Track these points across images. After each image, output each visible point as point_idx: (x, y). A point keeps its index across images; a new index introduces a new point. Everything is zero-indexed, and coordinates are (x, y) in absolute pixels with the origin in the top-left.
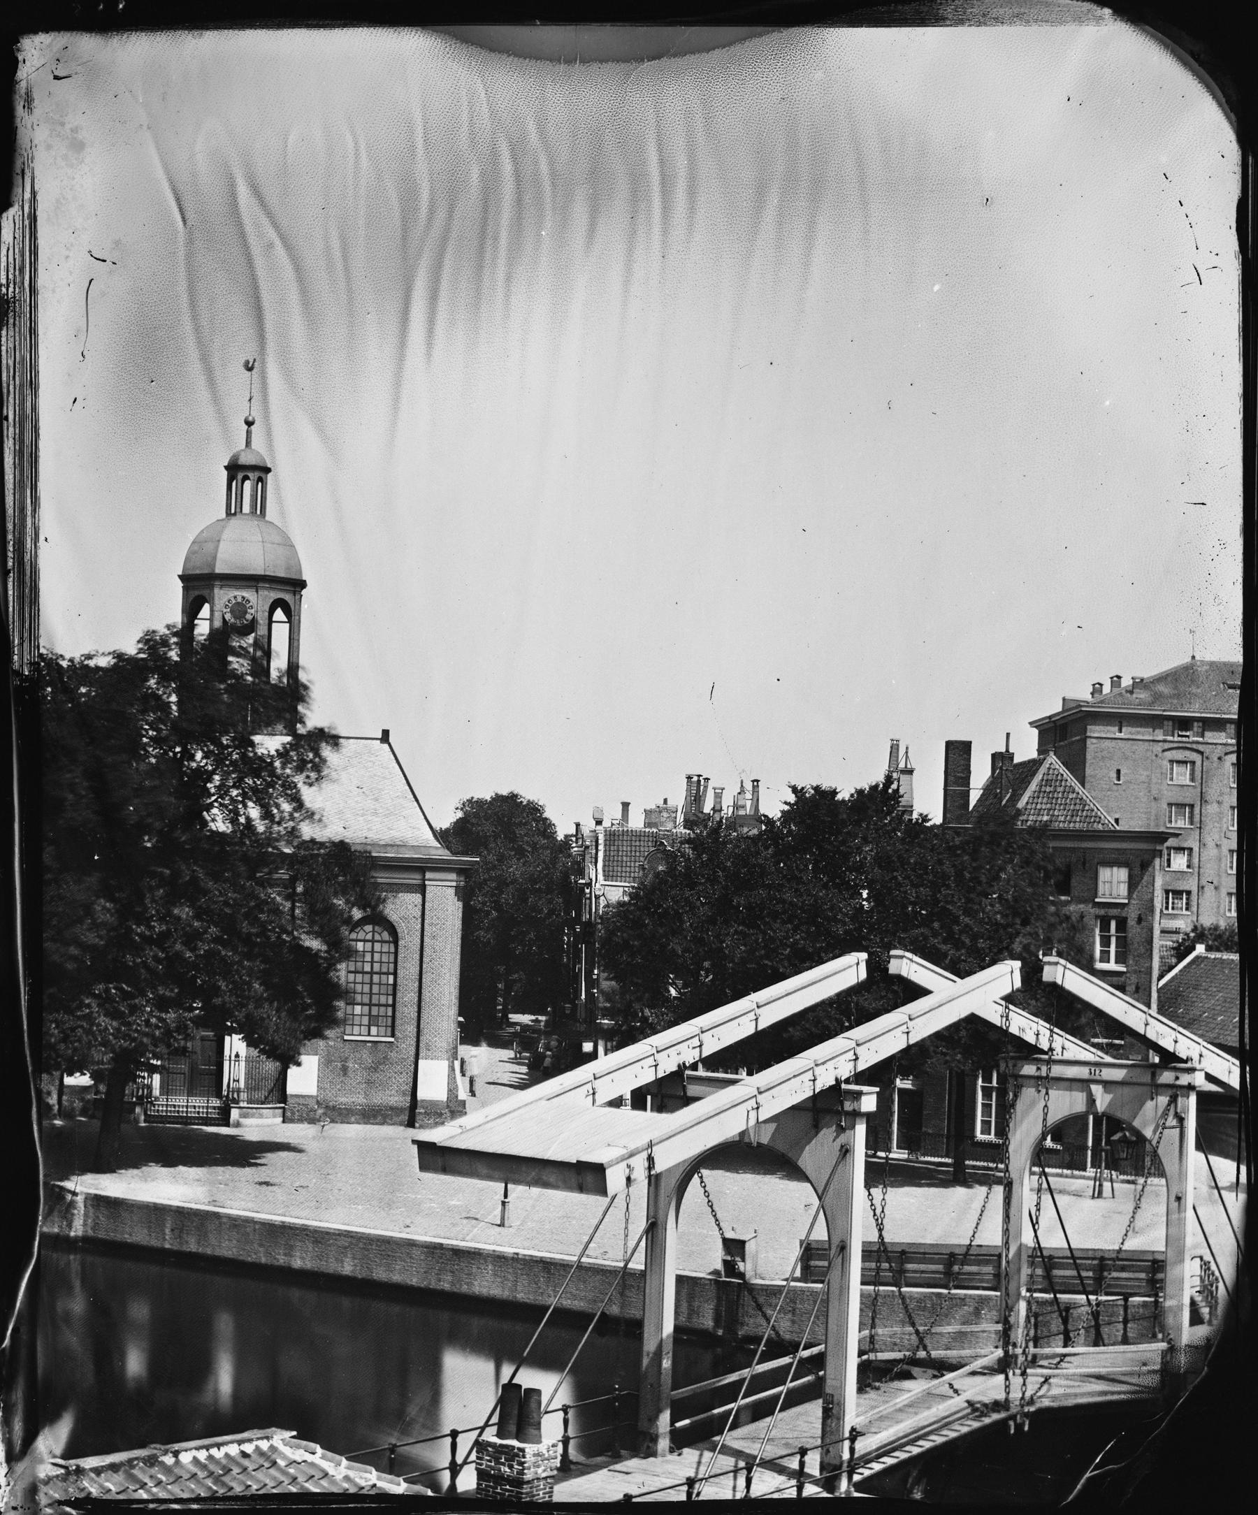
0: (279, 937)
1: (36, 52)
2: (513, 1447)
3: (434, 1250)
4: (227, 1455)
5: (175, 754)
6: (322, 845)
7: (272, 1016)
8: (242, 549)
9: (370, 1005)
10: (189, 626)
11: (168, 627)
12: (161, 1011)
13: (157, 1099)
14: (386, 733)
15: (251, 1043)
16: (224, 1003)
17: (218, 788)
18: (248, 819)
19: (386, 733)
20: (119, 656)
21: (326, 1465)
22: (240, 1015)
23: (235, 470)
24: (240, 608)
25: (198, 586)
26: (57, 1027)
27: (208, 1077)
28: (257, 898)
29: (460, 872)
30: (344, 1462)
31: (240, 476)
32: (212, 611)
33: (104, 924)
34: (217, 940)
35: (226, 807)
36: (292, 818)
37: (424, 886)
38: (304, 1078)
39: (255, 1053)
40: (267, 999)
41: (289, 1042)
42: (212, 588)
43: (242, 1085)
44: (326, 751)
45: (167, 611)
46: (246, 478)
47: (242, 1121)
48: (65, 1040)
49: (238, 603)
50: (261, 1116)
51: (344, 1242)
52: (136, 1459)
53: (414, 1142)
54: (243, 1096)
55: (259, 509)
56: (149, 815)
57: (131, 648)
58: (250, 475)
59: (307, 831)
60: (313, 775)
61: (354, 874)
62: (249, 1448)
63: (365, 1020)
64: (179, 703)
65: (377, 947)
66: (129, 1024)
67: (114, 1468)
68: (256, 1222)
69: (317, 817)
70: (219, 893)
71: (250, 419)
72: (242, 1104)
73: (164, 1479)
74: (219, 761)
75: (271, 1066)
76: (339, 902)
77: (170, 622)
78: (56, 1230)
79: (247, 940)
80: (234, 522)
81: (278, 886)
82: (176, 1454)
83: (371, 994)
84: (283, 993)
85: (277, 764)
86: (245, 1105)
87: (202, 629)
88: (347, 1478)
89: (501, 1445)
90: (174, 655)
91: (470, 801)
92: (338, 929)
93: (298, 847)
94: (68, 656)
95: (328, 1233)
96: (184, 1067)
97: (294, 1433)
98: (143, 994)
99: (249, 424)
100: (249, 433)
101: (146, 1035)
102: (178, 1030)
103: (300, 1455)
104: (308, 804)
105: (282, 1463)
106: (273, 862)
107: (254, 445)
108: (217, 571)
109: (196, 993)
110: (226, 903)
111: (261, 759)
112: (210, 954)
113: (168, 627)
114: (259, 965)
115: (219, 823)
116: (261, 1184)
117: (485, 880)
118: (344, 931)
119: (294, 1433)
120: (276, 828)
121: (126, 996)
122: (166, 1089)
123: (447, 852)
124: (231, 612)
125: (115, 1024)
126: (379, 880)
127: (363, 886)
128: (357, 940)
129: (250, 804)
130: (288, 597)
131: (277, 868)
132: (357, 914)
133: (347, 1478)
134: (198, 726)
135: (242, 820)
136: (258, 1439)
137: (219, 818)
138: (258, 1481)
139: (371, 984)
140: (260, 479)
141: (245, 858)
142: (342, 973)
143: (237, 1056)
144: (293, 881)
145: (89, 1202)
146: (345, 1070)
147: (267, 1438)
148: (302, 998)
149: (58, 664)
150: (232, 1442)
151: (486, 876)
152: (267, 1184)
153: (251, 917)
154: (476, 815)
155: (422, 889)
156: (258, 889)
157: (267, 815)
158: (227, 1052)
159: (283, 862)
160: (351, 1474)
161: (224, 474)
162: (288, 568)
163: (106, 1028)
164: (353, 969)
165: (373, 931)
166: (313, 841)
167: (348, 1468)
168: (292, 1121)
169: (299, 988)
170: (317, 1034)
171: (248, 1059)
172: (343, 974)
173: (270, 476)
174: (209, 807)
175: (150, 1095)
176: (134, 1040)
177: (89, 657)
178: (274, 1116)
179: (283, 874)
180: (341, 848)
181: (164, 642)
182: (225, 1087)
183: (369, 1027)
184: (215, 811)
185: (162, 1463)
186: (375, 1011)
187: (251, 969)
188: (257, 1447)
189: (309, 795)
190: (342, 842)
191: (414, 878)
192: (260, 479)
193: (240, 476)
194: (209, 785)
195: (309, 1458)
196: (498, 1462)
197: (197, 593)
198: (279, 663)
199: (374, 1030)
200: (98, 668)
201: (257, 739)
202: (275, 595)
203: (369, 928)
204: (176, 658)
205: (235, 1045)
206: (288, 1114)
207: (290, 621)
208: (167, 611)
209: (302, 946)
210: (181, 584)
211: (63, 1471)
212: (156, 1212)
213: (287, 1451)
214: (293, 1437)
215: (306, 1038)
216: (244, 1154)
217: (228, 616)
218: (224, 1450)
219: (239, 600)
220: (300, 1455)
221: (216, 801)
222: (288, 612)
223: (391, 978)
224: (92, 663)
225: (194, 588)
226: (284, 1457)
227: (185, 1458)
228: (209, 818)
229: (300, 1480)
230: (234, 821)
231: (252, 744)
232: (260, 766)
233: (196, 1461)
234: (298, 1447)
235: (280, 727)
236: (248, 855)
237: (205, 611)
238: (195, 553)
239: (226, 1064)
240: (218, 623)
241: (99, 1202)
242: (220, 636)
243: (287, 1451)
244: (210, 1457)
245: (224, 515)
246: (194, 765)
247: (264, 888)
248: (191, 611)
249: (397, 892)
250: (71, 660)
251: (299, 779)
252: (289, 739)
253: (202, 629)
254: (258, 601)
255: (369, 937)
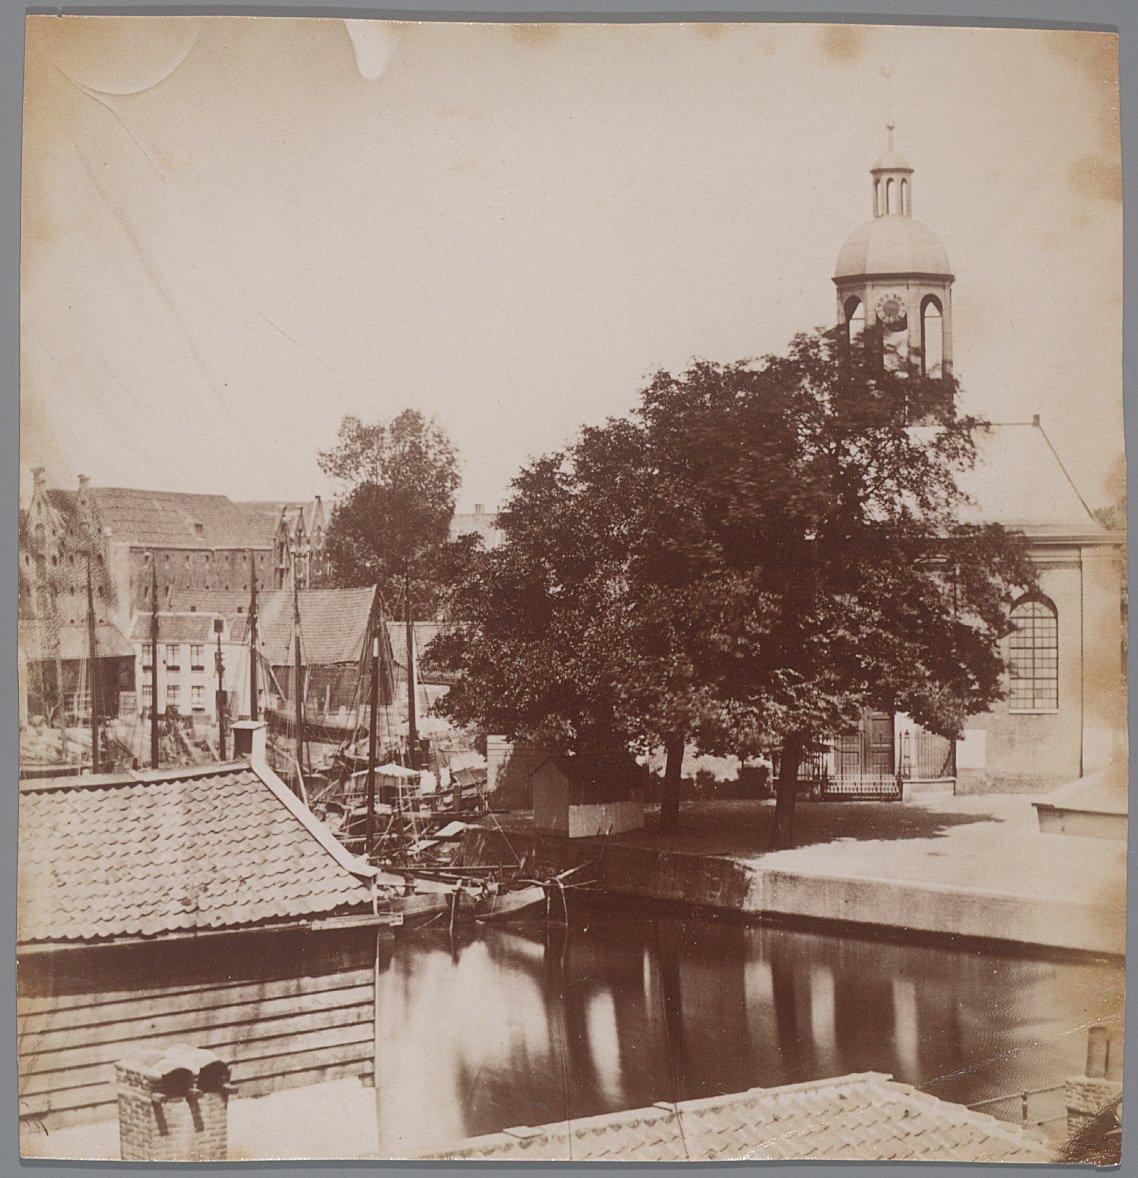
1: (43, 39)
5: (830, 450)
8: (890, 249)
10: (845, 327)
12: (827, 693)
13: (832, 777)
14: (1037, 417)
16: (887, 683)
19: (1037, 417)
24: (891, 307)
25: (850, 287)
28: (915, 580)
34: (880, 624)
35: (882, 497)
36: (948, 503)
37: (1081, 562)
41: (952, 719)
48: (736, 724)
49: (890, 302)
52: (737, 1101)
53: (1033, 805)
55: (905, 208)
57: (784, 352)
59: (964, 515)
62: (845, 1091)
71: (891, 125)
72: (912, 780)
74: (875, 455)
75: (940, 743)
76: (996, 580)
77: (818, 325)
79: (910, 621)
81: (937, 569)
84: (945, 671)
90: (825, 355)
92: (995, 607)
94: (723, 363)
96: (858, 746)
97: (891, 1076)
98: (809, 678)
102: (845, 711)
105: (876, 1104)
110: (886, 589)
118: (1005, 608)
121: (793, 680)
122: (841, 769)
125: (784, 708)
127: (1018, 566)
134: (854, 420)
135: (898, 509)
141: (903, 545)
142: (1004, 648)
143: (907, 733)
144: (951, 562)
145: (767, 879)
146: (1011, 741)
152: (937, 854)
153: (912, 600)
156: (918, 575)
165: (1034, 609)
173: (913, 175)
176: (803, 722)
177: (743, 363)
178: (947, 789)
182: (897, 765)
184: (871, 501)
189: (961, 480)
192: (904, 180)
194: (865, 477)
197: (850, 294)
198: (933, 358)
200: (753, 373)
203: (1029, 605)
206: (958, 787)
207: (942, 315)
216: (925, 825)
217: (881, 314)
219: (891, 298)
221: (872, 492)
222: (939, 306)
224: (747, 369)
225: (849, 289)
228: (865, 508)
230: (891, 511)
232: (915, 457)
233: (794, 1104)
235: (931, 418)
236: (905, 542)
237: (859, 312)
240: (872, 322)
244: (809, 1099)
245: (870, 215)
246: (849, 459)
247: (923, 572)
251: (952, 466)
253: (856, 327)
254: (909, 297)
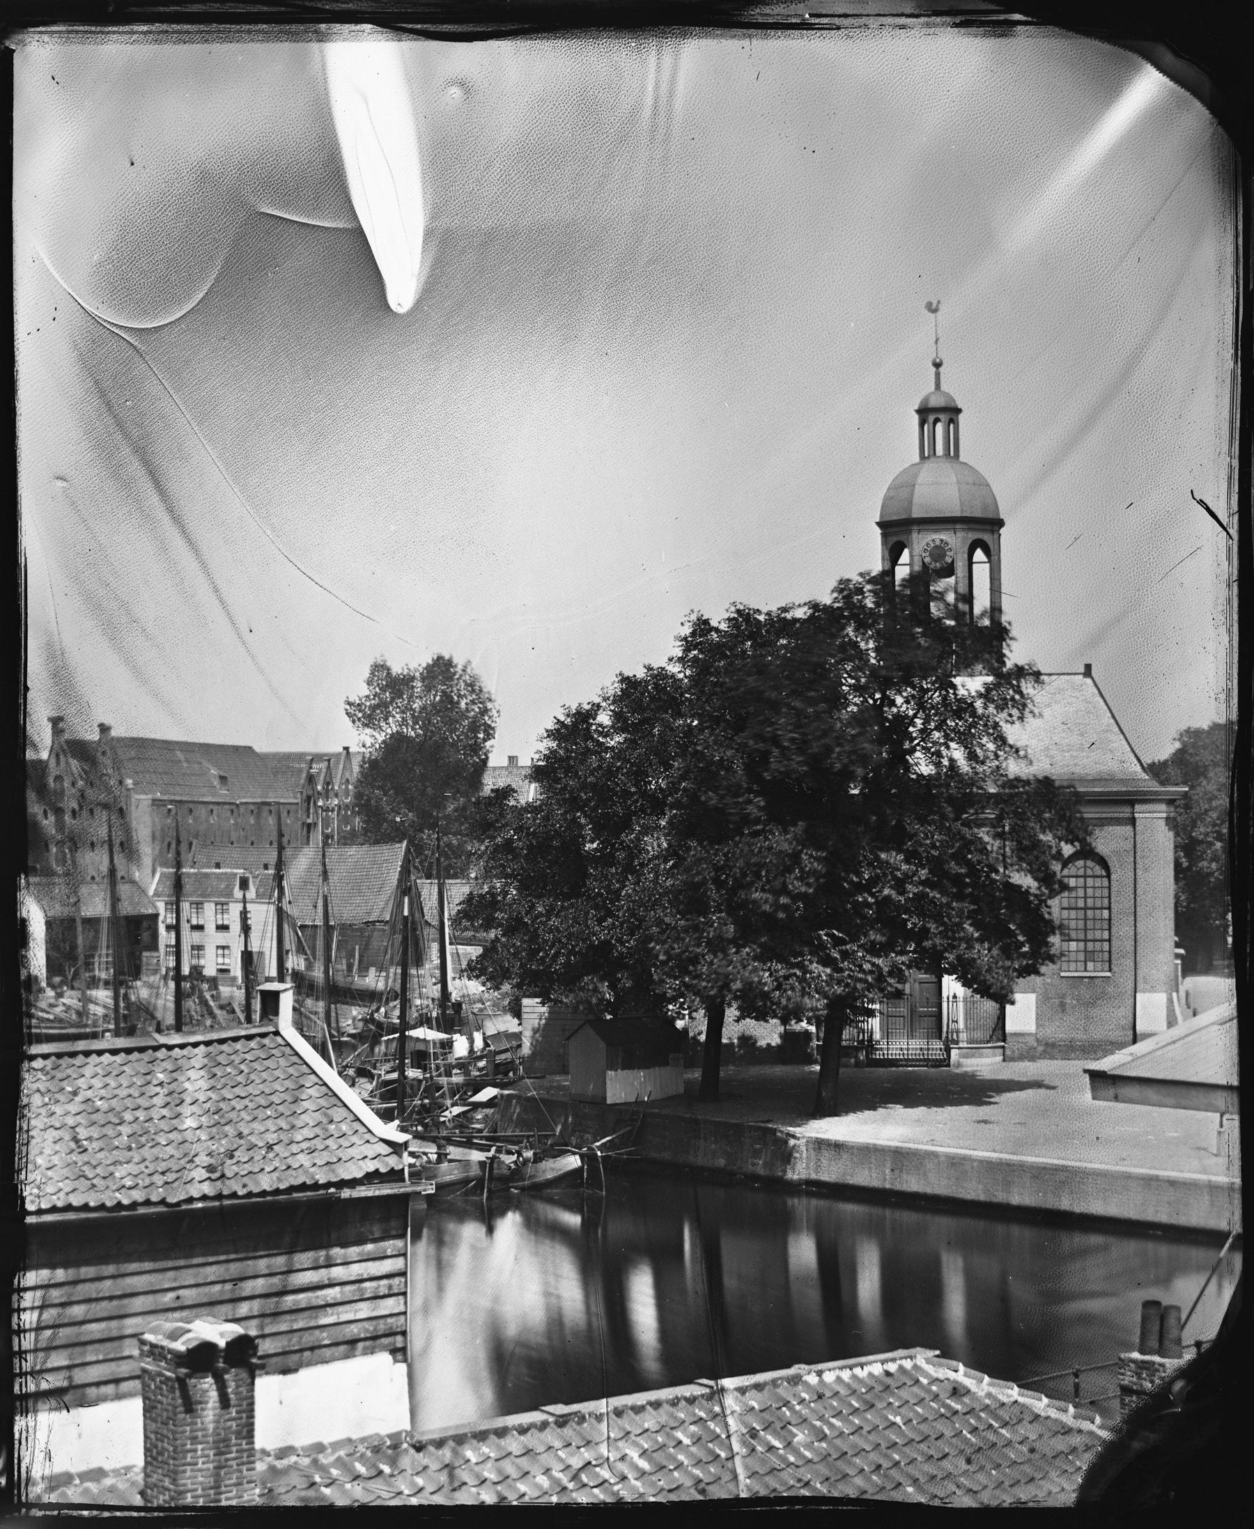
0: (988, 876)
2: (1153, 1363)
3: (1149, 1182)
4: (870, 1374)
5: (875, 701)
6: (1028, 782)
7: (983, 954)
8: (939, 491)
9: (1086, 941)
10: (889, 573)
11: (861, 575)
14: (1088, 668)
15: (966, 984)
16: (934, 946)
17: (921, 731)
18: (952, 760)
19: (1088, 668)
20: (815, 606)
21: (969, 1383)
22: (951, 957)
23: (925, 413)
24: (939, 551)
25: (896, 531)
26: (771, 975)
27: (932, 1020)
28: (963, 838)
29: (1170, 802)
30: (987, 1378)
31: (931, 418)
32: (911, 556)
33: (814, 872)
36: (997, 757)
38: (1023, 1013)
39: (969, 992)
40: (977, 940)
42: (910, 532)
43: (961, 1025)
44: (1028, 687)
45: (869, 556)
46: (937, 420)
47: (963, 1061)
50: (981, 1056)
51: (1062, 1176)
54: (963, 1036)
55: (952, 452)
56: (852, 762)
58: (942, 416)
59: (1014, 768)
60: (1015, 712)
61: (1059, 807)
62: (892, 1367)
63: (1081, 957)
64: (877, 649)
65: (1090, 882)
66: (841, 970)
67: (758, 1387)
68: (975, 1160)
69: (1022, 753)
70: (930, 837)
72: (961, 1045)
73: (807, 1397)
75: (989, 1006)
76: (1047, 837)
78: (721, 1162)
79: (957, 880)
80: (928, 465)
82: (820, 1373)
83: (1086, 930)
84: (994, 932)
85: (979, 704)
86: (965, 1045)
87: (902, 572)
88: (989, 1395)
89: (1143, 1362)
91: (1188, 731)
93: (1003, 786)
94: (764, 610)
95: (1044, 1168)
96: (903, 1010)
97: (938, 1352)
98: (854, 939)
99: (937, 365)
100: (938, 375)
101: (860, 980)
103: (942, 1373)
104: (1011, 741)
105: (924, 1381)
106: (979, 802)
107: (944, 387)
108: (914, 516)
109: (909, 935)
111: (961, 701)
112: (920, 897)
113: (861, 575)
114: (968, 906)
115: (923, 766)
116: (979, 1122)
117: (1206, 811)
119: (938, 1352)
120: (980, 769)
121: (837, 942)
122: (887, 1033)
123: (1156, 784)
124: (931, 555)
125: (828, 971)
126: (1086, 816)
128: (1069, 877)
129: (953, 745)
130: (986, 537)
131: (983, 808)
132: (1068, 850)
133: (989, 1395)
135: (945, 762)
136: (901, 1358)
137: (922, 762)
138: (900, 1398)
139: (1086, 919)
140: (951, 421)
141: (951, 800)
142: (1056, 908)
143: (955, 997)
145: (811, 1146)
147: (911, 1358)
148: (1015, 936)
149: (755, 619)
150: (875, 1362)
151: (1207, 806)
152: (985, 1122)
153: (959, 857)
154: (1194, 745)
155: (1133, 822)
156: (965, 830)
157: (972, 756)
158: (945, 995)
159: (988, 802)
160: (993, 1390)
161: (916, 419)
162: (985, 508)
163: (820, 976)
164: (1066, 905)
165: (1085, 867)
166: (1018, 779)
167: (990, 1385)
168: (1013, 1059)
169: (1013, 928)
170: (1032, 970)
171: (965, 1000)
172: (1055, 911)
174: (912, 751)
175: (871, 1039)
176: (847, 985)
177: (785, 610)
179: (990, 814)
180: (1046, 783)
181: (860, 591)
182: (945, 1029)
183: (1085, 962)
184: (918, 754)
185: (806, 1383)
186: (1090, 945)
187: (961, 910)
188: (901, 1368)
189: (1013, 733)
190: (1046, 778)
191: (1124, 812)
192: (951, 421)
193: (931, 418)
195: (952, 1375)
196: (1139, 1377)
197: (895, 539)
198: (982, 601)
199: (1090, 965)
200: (795, 620)
201: (957, 681)
202: (973, 536)
203: (1080, 863)
204: (870, 605)
205: (951, 985)
206: (1008, 1052)
207: (990, 561)
208: (869, 556)
209: (1012, 884)
210: (879, 531)
211: (708, 1390)
212: (867, 1152)
213: (929, 1369)
214: (937, 1356)
215: (1020, 975)
216: (975, 1092)
217: (927, 560)
218: (867, 1369)
219: (938, 543)
220: (942, 1373)
222: (987, 552)
223: (1106, 913)
224: (789, 616)
226: (927, 1375)
227: (829, 1377)
229: (942, 1396)
230: (938, 765)
231: (954, 687)
232: (964, 708)
233: (839, 1379)
234: (940, 1365)
236: (953, 796)
237: (905, 557)
238: (892, 498)
239: (945, 1005)
240: (917, 568)
241: (820, 1145)
242: (921, 580)
243: (929, 1369)
244: (854, 1377)
245: (917, 459)
246: (895, 710)
247: (971, 828)
248: (893, 554)
249: (1103, 825)
250: (768, 614)
251: (1001, 717)
252: (990, 679)
253: (902, 572)
254: (955, 541)
255: (1081, 872)
